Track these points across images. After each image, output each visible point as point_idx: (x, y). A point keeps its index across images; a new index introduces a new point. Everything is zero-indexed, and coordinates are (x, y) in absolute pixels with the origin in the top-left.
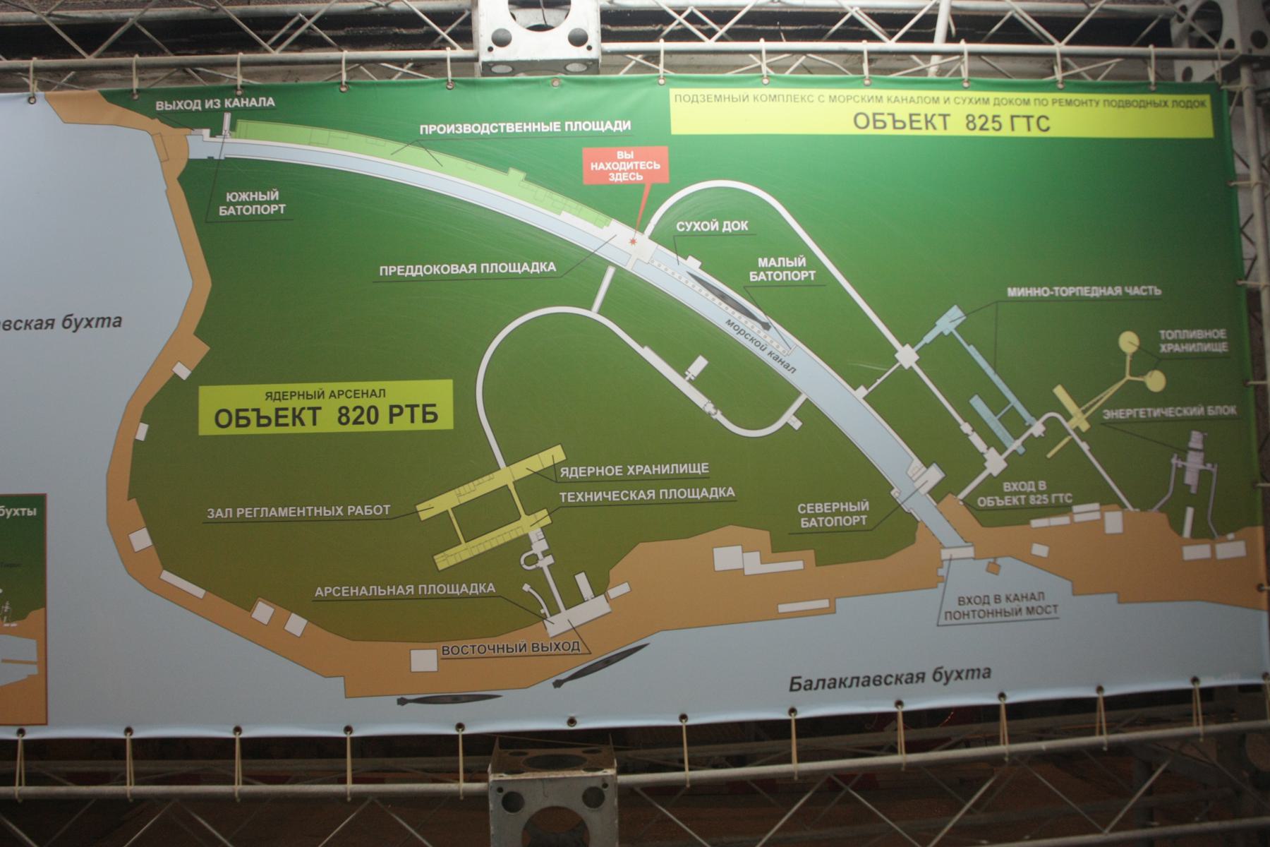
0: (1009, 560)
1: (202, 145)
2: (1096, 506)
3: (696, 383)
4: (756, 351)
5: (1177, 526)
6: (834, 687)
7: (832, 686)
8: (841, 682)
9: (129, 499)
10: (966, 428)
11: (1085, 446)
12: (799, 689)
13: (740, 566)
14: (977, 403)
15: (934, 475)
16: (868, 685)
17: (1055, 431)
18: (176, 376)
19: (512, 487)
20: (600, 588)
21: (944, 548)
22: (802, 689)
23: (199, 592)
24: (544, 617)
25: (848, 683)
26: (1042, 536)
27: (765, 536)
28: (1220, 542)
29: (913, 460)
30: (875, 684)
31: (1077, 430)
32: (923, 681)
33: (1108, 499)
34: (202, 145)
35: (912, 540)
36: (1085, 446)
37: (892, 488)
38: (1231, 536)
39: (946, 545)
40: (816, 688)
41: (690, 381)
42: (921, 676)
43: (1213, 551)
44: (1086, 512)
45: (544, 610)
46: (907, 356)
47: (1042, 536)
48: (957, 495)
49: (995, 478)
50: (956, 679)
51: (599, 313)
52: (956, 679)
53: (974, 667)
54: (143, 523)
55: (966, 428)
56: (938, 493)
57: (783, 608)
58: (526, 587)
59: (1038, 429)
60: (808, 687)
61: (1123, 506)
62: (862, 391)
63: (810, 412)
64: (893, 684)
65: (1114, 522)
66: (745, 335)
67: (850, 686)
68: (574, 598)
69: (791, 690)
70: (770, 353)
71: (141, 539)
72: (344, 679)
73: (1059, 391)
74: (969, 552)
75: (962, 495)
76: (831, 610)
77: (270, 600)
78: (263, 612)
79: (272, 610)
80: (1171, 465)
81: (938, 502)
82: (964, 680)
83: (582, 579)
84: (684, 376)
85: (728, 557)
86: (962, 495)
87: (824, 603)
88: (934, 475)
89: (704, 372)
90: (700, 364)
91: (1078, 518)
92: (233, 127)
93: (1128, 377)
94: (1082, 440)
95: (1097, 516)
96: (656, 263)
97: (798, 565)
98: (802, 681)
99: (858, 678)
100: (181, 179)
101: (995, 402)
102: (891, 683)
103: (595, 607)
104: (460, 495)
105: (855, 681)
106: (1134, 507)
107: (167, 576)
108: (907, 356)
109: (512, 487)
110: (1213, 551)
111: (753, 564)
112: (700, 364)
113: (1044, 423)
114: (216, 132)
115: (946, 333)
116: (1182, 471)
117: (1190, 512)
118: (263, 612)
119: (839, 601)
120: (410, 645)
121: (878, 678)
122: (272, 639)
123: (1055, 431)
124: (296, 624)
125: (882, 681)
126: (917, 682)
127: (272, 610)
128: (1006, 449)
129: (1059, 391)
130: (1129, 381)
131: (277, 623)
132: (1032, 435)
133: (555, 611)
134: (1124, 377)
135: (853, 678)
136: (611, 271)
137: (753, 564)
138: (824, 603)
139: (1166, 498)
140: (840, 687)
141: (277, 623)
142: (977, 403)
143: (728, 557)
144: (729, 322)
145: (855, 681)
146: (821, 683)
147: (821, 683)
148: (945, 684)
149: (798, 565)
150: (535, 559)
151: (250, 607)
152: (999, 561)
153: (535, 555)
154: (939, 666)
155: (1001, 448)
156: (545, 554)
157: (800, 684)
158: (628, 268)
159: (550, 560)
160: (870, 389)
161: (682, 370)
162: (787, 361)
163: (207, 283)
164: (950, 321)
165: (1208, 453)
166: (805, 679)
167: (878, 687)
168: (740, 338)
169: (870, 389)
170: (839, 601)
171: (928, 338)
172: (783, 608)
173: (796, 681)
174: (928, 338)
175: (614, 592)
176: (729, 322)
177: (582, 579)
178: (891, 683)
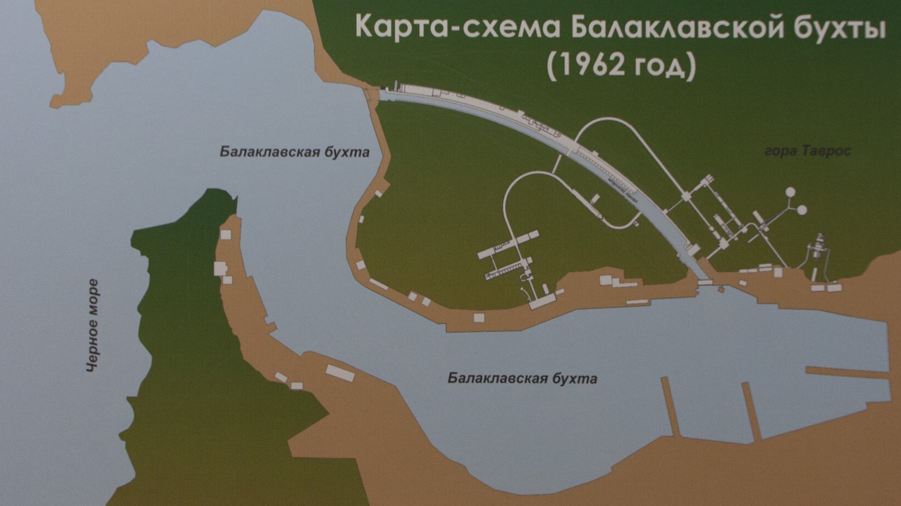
0: (729, 287)
1: (386, 95)
2: (770, 265)
3: (595, 206)
4: (621, 192)
5: (809, 276)
6: (481, 382)
7: (479, 380)
8: (485, 379)
9: (356, 248)
10: (712, 228)
11: (766, 238)
12: (455, 382)
13: (611, 284)
14: (718, 219)
15: (696, 248)
16: (505, 382)
17: (752, 231)
18: (376, 196)
19: (517, 247)
20: (552, 290)
21: (700, 280)
22: (457, 382)
23: (386, 288)
24: (529, 301)
25: (491, 379)
26: (744, 277)
27: (622, 271)
28: (830, 284)
29: (687, 241)
30: (510, 382)
31: (763, 231)
32: (546, 382)
33: (775, 262)
34: (386, 95)
35: (685, 276)
36: (766, 238)
37: (677, 253)
38: (835, 282)
39: (700, 279)
40: (468, 382)
41: (592, 205)
42: (544, 378)
43: (826, 288)
44: (765, 267)
45: (529, 298)
46: (686, 196)
47: (744, 277)
48: (706, 257)
49: (724, 251)
50: (570, 382)
51: (555, 174)
52: (570, 382)
53: (585, 375)
54: (361, 257)
55: (712, 228)
56: (697, 256)
57: (629, 302)
58: (522, 289)
59: (745, 230)
60: (462, 380)
61: (783, 266)
62: (666, 211)
63: (643, 220)
64: (524, 383)
65: (778, 272)
66: (616, 185)
67: (492, 382)
68: (541, 294)
69: (449, 381)
70: (627, 194)
71: (361, 265)
72: (446, 326)
73: (756, 214)
74: (710, 282)
75: (708, 257)
76: (649, 304)
77: (415, 291)
78: (413, 296)
79: (416, 296)
80: (807, 248)
81: (697, 260)
82: (577, 384)
83: (545, 286)
84: (590, 203)
85: (605, 280)
86: (708, 257)
87: (646, 301)
88: (696, 248)
89: (599, 200)
90: (596, 198)
91: (761, 270)
92: (398, 87)
93: (789, 208)
94: (766, 235)
95: (770, 269)
96: (579, 153)
97: (635, 284)
98: (458, 376)
99: (498, 376)
100: (376, 110)
101: (725, 217)
102: (522, 382)
103: (551, 298)
104: (495, 249)
105: (496, 378)
106: (788, 266)
107: (372, 281)
108: (686, 196)
109: (517, 247)
110: (826, 288)
111: (616, 283)
112: (596, 198)
113: (748, 227)
114: (392, 89)
115: (705, 186)
116: (812, 251)
117: (815, 270)
118: (413, 296)
119: (653, 301)
120: (473, 311)
121: (512, 378)
122: (416, 308)
123: (752, 231)
124: (427, 302)
125: (516, 379)
126: (541, 382)
127: (416, 296)
128: (729, 238)
129: (756, 214)
130: (789, 210)
131: (419, 301)
132: (741, 233)
133: (534, 299)
134: (786, 207)
135: (494, 376)
136: (560, 156)
137: (616, 283)
138: (646, 301)
139: (804, 263)
140: (485, 382)
141: (419, 301)
142: (718, 219)
143: (605, 280)
144: (609, 180)
145: (496, 378)
146: (471, 378)
147: (471, 378)
148: (562, 385)
149: (635, 284)
150: (525, 277)
151: (407, 294)
152: (724, 287)
153: (526, 276)
154: (559, 372)
155: (727, 238)
156: (530, 275)
157: (456, 378)
158: (568, 155)
159: (532, 278)
160: (670, 210)
161: (589, 199)
162: (634, 197)
163: (389, 156)
164: (705, 182)
165: (825, 245)
166: (461, 375)
167: (511, 384)
168: (614, 187)
169: (670, 210)
170: (653, 301)
171: (696, 188)
172: (629, 302)
173: (453, 375)
174: (696, 188)
175: (558, 292)
176: (609, 180)
177: (545, 286)
178: (522, 382)
